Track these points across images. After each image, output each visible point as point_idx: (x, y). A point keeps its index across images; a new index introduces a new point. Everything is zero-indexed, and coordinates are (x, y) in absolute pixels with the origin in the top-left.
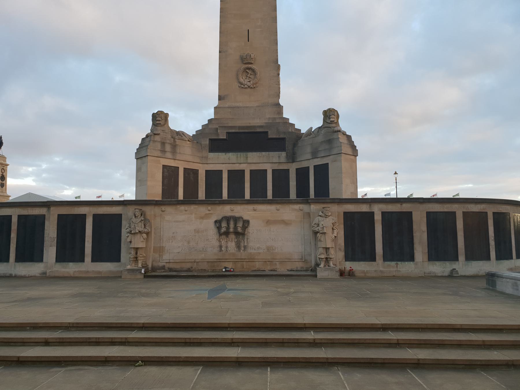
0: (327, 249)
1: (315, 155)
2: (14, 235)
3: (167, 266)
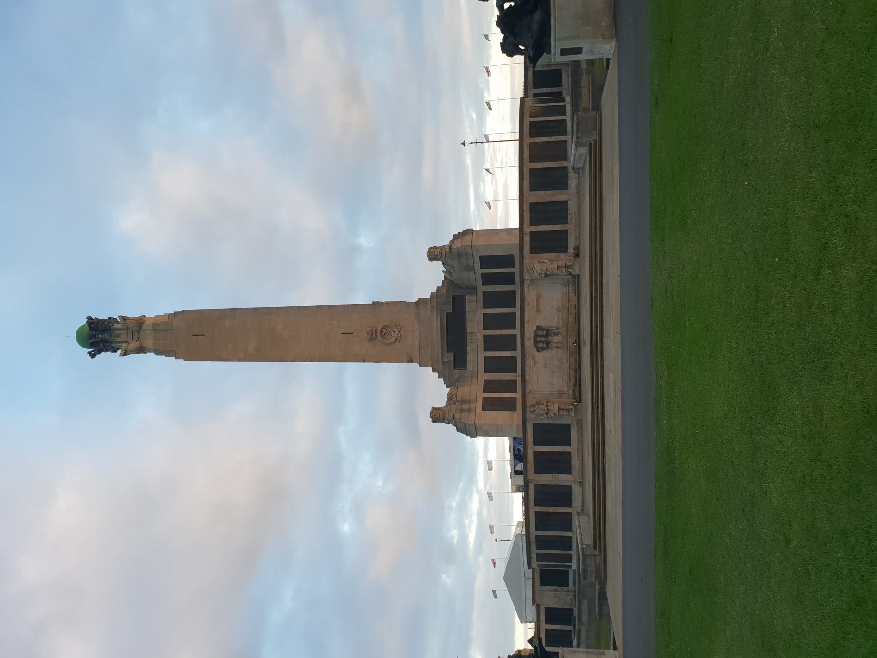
0: (558, 267)
1: (471, 269)
2: (551, 510)
3: (572, 388)
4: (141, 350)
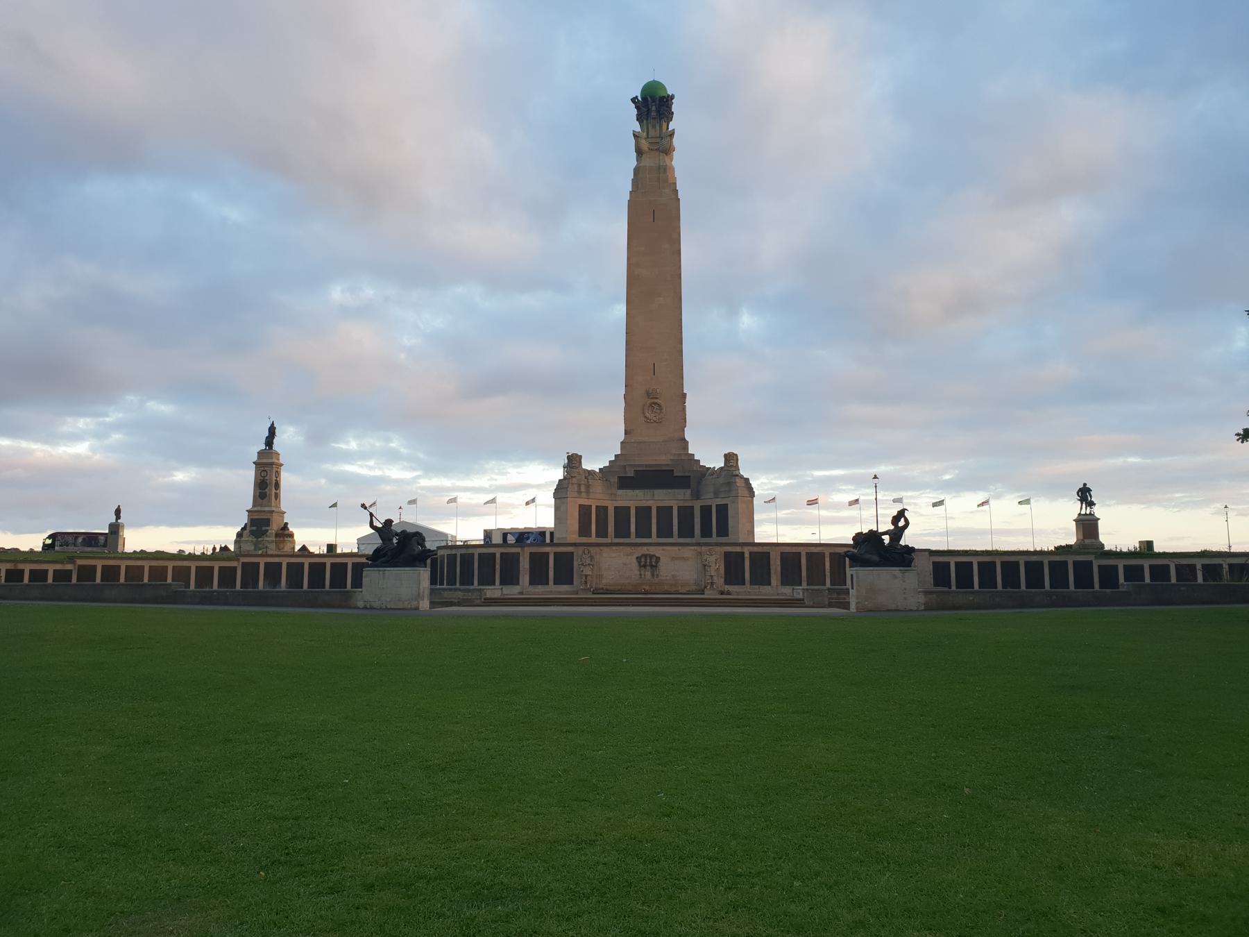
1: (716, 495)
2: (498, 567)
4: (639, 152)
